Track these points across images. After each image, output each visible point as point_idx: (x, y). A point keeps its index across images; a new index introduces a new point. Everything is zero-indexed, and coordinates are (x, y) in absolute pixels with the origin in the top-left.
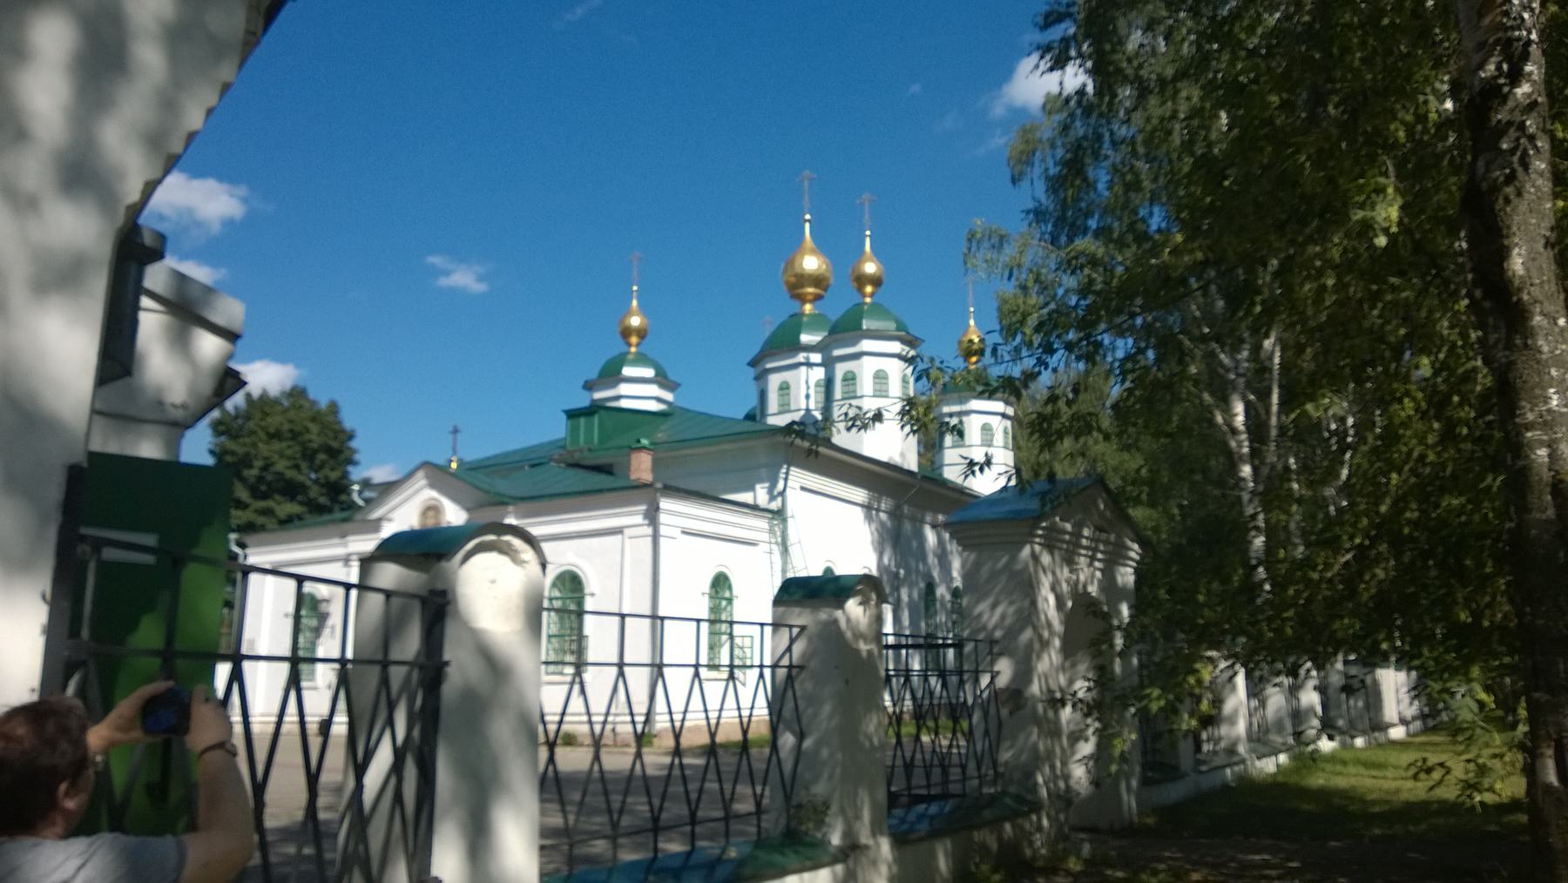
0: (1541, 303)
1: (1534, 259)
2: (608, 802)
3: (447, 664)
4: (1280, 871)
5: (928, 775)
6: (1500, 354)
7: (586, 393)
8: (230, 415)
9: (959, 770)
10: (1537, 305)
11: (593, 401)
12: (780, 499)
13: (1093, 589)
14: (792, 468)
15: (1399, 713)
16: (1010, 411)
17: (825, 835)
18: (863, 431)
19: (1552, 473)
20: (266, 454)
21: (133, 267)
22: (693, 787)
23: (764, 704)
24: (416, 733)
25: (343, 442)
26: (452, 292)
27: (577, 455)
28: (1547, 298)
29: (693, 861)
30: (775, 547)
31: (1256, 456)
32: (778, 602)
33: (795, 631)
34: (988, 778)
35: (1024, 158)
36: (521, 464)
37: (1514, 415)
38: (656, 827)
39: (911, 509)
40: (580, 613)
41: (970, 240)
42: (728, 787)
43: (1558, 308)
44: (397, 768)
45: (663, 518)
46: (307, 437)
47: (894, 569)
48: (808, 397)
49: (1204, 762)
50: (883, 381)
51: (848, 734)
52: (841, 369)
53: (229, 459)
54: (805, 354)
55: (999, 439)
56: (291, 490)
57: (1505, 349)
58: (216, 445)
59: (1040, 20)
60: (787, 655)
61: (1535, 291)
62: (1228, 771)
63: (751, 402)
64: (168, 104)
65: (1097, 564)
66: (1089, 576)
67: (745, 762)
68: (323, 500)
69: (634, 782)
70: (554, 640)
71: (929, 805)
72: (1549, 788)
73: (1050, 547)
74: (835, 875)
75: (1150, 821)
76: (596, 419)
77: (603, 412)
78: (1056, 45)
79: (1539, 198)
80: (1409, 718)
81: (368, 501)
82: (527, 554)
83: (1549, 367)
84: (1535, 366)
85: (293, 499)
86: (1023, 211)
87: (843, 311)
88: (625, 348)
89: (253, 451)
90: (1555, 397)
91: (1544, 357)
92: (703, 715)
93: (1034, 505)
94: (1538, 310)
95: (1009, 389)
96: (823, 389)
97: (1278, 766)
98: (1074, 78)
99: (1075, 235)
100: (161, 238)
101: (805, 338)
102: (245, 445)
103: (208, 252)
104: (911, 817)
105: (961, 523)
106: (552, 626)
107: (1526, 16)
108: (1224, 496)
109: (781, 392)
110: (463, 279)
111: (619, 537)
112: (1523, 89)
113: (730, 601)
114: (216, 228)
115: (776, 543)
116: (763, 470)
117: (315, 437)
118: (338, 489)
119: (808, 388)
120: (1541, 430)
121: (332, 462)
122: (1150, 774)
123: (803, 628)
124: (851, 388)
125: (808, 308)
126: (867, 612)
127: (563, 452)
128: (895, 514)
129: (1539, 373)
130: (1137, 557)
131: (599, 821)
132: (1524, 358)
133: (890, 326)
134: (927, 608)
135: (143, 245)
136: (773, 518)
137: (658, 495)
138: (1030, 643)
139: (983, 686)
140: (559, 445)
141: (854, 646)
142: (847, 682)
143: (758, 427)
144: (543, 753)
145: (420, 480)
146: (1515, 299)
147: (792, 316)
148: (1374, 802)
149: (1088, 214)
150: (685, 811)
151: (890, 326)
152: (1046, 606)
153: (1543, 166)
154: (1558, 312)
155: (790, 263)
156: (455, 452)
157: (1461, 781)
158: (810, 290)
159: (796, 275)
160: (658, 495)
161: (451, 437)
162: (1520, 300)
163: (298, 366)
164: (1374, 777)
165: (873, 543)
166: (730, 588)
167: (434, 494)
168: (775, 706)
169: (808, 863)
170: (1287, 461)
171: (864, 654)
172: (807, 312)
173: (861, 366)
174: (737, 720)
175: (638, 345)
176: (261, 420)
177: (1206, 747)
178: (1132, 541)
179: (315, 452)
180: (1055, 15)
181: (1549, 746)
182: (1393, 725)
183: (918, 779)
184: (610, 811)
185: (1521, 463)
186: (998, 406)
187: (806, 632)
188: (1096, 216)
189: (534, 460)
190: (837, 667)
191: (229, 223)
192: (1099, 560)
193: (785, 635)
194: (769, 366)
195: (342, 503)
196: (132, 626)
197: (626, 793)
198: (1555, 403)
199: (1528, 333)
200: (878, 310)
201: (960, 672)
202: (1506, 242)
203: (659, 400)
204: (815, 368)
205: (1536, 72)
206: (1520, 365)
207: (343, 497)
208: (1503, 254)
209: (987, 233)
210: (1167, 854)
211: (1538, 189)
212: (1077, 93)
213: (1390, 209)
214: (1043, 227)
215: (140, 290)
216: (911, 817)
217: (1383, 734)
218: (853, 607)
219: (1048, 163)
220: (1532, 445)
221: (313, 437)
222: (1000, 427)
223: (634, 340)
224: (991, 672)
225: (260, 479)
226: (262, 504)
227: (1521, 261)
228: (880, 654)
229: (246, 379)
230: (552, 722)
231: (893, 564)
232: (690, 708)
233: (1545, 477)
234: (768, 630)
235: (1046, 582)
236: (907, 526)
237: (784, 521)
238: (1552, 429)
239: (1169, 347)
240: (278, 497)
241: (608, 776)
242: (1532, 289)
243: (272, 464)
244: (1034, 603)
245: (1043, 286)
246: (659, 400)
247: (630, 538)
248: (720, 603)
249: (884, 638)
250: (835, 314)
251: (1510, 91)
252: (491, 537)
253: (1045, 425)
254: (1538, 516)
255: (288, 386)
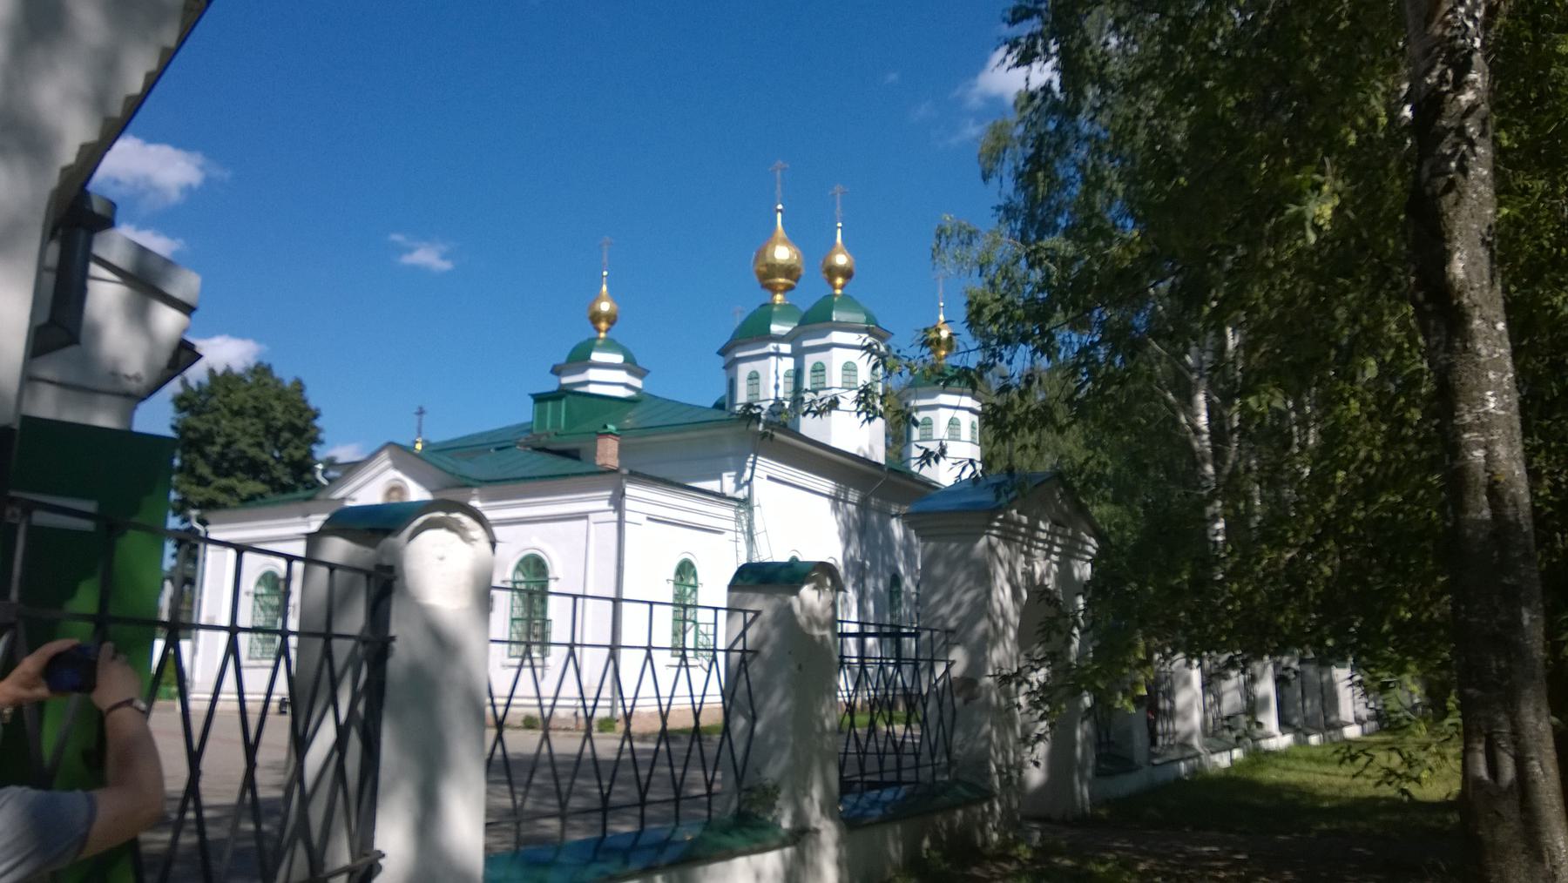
0: (1481, 307)
1: (1474, 264)
2: (557, 784)
3: (393, 639)
4: (1228, 863)
5: (881, 763)
6: (1440, 357)
7: (554, 378)
8: (192, 389)
9: (912, 758)
10: (1477, 309)
11: (561, 385)
12: (746, 488)
13: (1050, 583)
14: (759, 458)
15: (1355, 712)
16: (977, 406)
17: (775, 818)
18: (818, 416)
19: (1488, 474)
20: (228, 430)
21: (82, 235)
22: (644, 772)
23: (718, 692)
24: (361, 708)
25: (308, 421)
26: (415, 269)
27: (544, 439)
28: (1487, 302)
29: (643, 841)
30: (740, 535)
31: (1218, 456)
32: (732, 587)
33: (750, 616)
34: (942, 766)
35: (994, 154)
36: (486, 447)
37: (1453, 417)
38: (606, 808)
39: (878, 500)
40: (544, 593)
41: (939, 236)
42: (678, 771)
43: (1497, 313)
44: (340, 744)
45: (629, 504)
46: (271, 415)
47: (859, 560)
48: (777, 387)
49: (1156, 755)
50: (852, 373)
51: (804, 717)
52: (810, 360)
53: (191, 435)
54: (775, 345)
55: (965, 432)
56: (255, 469)
57: (1445, 352)
58: (179, 421)
59: (1008, 15)
60: (742, 640)
61: (1475, 295)
62: (1182, 765)
63: (721, 391)
64: (108, 64)
65: (1054, 557)
66: (1043, 567)
67: (696, 745)
68: (286, 480)
69: (579, 765)
70: (517, 623)
71: (882, 792)
72: (1479, 781)
73: (1008, 537)
74: (783, 858)
75: (1103, 812)
76: (563, 403)
77: (570, 396)
78: (1023, 40)
79: (1480, 204)
80: (1365, 718)
81: (330, 480)
82: (477, 532)
83: (1487, 371)
84: (1474, 369)
85: (255, 478)
86: (993, 208)
87: (813, 302)
88: (593, 334)
89: (215, 428)
90: (1492, 399)
91: (1482, 360)
92: (655, 701)
93: (988, 497)
94: (1477, 313)
95: (966, 380)
96: (792, 380)
97: (1232, 761)
98: (1043, 73)
99: (1045, 233)
100: (112, 206)
101: (776, 328)
102: (208, 421)
103: (163, 221)
104: (864, 802)
105: (918, 513)
106: (515, 609)
107: (1470, 24)
108: (1187, 495)
109: (751, 382)
110: (426, 257)
111: (584, 522)
112: (1467, 97)
113: (695, 588)
114: (175, 196)
115: (743, 532)
116: (730, 459)
117: (279, 415)
118: (302, 468)
119: (777, 378)
120: (1478, 431)
121: (296, 441)
122: (1103, 766)
123: (757, 613)
124: (820, 379)
125: (779, 298)
126: (822, 597)
127: (529, 436)
128: (863, 506)
129: (1477, 376)
130: (1094, 552)
131: (552, 804)
132: (1463, 361)
133: (860, 318)
134: (892, 601)
135: (93, 212)
136: (739, 507)
137: (624, 481)
138: (985, 636)
139: (938, 676)
140: (525, 428)
141: (807, 632)
142: (800, 667)
143: (725, 416)
144: (491, 734)
145: (384, 460)
146: (1455, 302)
147: (763, 305)
148: (1324, 798)
149: (1058, 211)
150: (634, 793)
151: (860, 318)
152: (1001, 595)
153: (1485, 173)
154: (1496, 316)
155: (761, 253)
156: (420, 433)
157: (1383, 768)
158: (781, 280)
159: (767, 265)
160: (624, 481)
161: (416, 418)
162: (1460, 303)
163: (257, 340)
164: (1326, 774)
165: (839, 533)
166: (695, 575)
167: (398, 475)
168: (728, 694)
169: (757, 846)
170: (1248, 462)
171: (818, 639)
172: (778, 302)
173: (831, 358)
174: (690, 706)
175: (607, 331)
176: (224, 396)
177: (1160, 740)
178: (1090, 535)
179: (280, 430)
180: (1024, 11)
181: (1480, 742)
182: (1349, 724)
183: (872, 763)
184: (559, 793)
185: (1458, 464)
186: (967, 401)
187: (760, 617)
188: (1066, 215)
189: (499, 443)
190: (790, 653)
191: (188, 190)
192: (1056, 554)
193: (739, 620)
194: (739, 355)
195: (305, 483)
196: (70, 592)
197: (574, 776)
198: (1492, 405)
199: (1467, 336)
200: (849, 302)
201: (916, 662)
202: (1448, 247)
203: (627, 386)
204: (785, 359)
205: (1480, 80)
206: (1459, 368)
207: (308, 476)
208: (1445, 258)
209: (957, 228)
210: (1117, 844)
211: (1480, 194)
212: (1042, 89)
213: (1323, 207)
214: (1013, 225)
215: (89, 257)
216: (864, 802)
217: (1338, 732)
218: (808, 593)
219: (1015, 158)
220: (1469, 447)
221: (278, 415)
222: (967, 421)
223: (603, 325)
224: (947, 661)
225: (222, 455)
226: (224, 482)
227: (1462, 265)
228: (835, 642)
229: (201, 352)
230: (501, 705)
231: (858, 554)
232: (640, 695)
233: (1481, 478)
234: (722, 615)
235: (1001, 574)
236: (874, 518)
237: (751, 509)
238: (1488, 431)
239: (1119, 338)
240: (240, 475)
241: (557, 759)
242: (1472, 293)
243: (234, 442)
244: (988, 593)
245: (1012, 282)
246: (627, 386)
247: (595, 523)
248: (685, 590)
249: (839, 624)
250: (805, 305)
251: (1454, 98)
252: (440, 514)
253: (999, 416)
254: (1474, 515)
255: (252, 364)
